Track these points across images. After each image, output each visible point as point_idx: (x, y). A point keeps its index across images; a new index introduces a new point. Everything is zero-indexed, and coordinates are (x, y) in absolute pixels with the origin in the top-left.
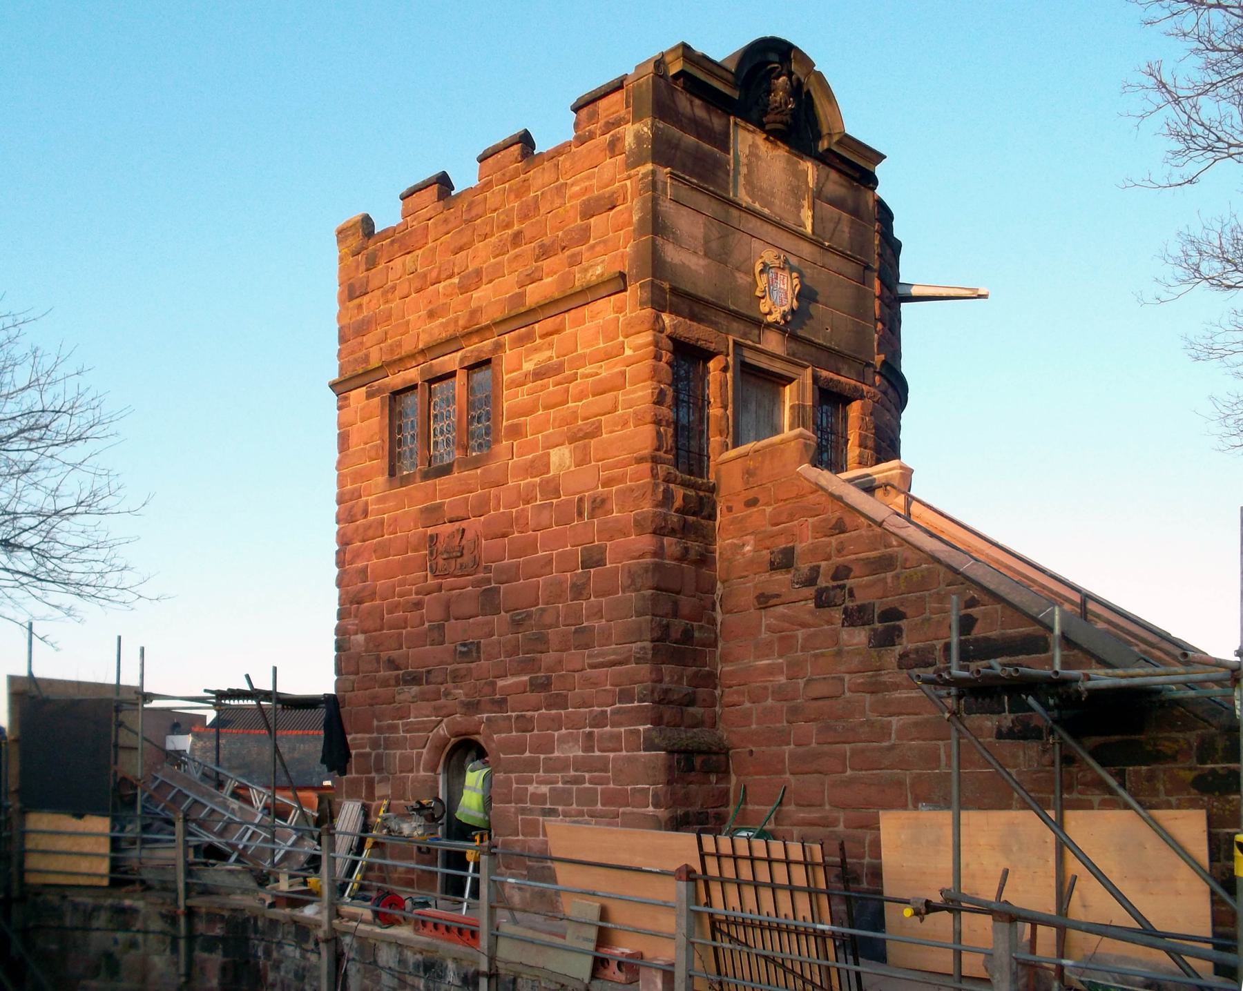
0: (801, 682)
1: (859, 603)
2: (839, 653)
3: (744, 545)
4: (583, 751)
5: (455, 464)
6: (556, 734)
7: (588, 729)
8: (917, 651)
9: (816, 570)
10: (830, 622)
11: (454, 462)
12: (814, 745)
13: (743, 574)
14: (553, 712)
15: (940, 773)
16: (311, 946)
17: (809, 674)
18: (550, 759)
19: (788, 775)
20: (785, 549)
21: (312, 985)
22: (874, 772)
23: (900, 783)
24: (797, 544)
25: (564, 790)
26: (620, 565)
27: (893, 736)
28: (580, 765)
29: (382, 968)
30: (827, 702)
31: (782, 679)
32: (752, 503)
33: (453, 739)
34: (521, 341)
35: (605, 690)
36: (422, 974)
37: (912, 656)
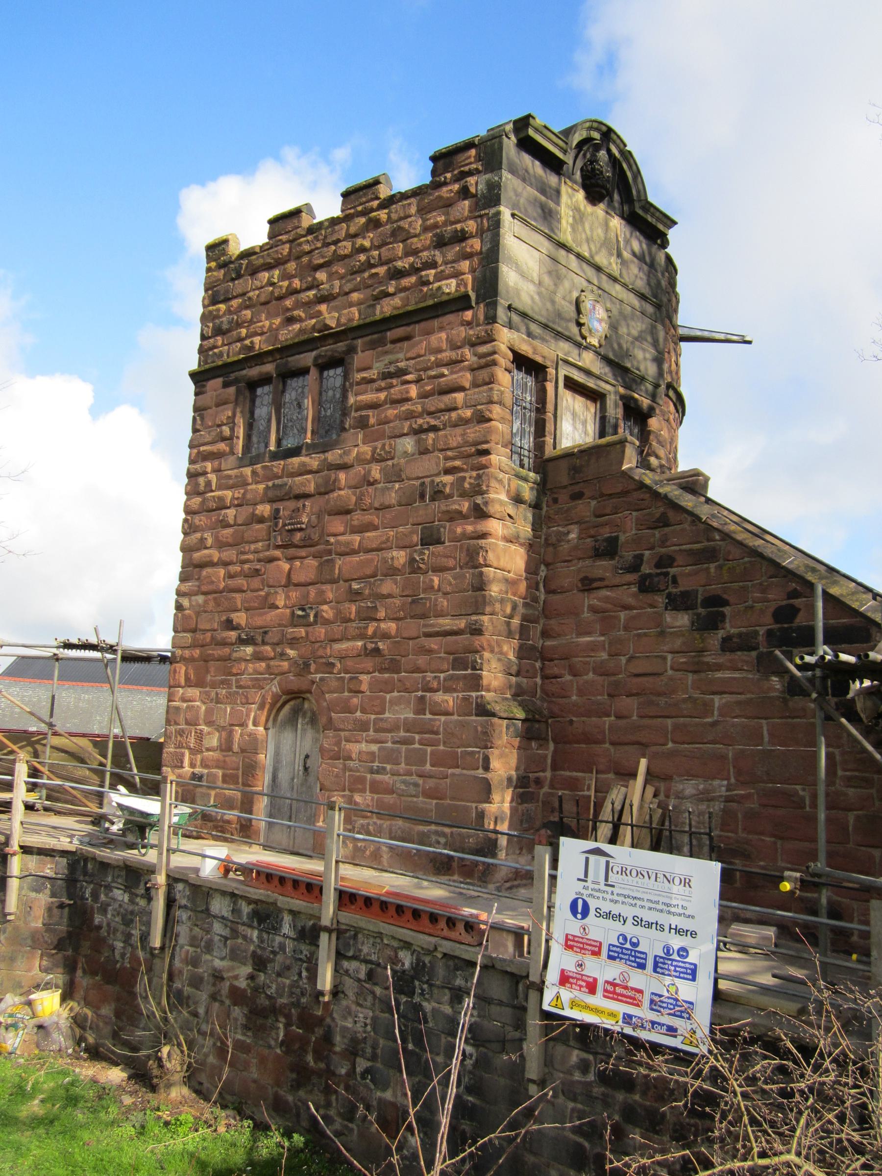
0: (623, 659)
1: (681, 589)
2: (662, 634)
3: (569, 532)
4: (415, 714)
5: (304, 448)
6: (388, 696)
7: (420, 693)
8: (740, 635)
9: (639, 558)
10: (652, 606)
11: (302, 445)
12: (635, 718)
13: (567, 558)
14: (386, 675)
15: (763, 750)
16: (141, 891)
17: (631, 652)
18: (382, 719)
19: (607, 745)
20: (610, 537)
22: (697, 746)
23: (723, 757)
25: (392, 750)
26: (459, 544)
27: (716, 713)
28: (409, 726)
29: (215, 917)
30: (650, 679)
31: (604, 655)
32: (577, 496)
33: (284, 697)
34: (372, 346)
35: (440, 657)
36: (255, 924)
37: (735, 640)
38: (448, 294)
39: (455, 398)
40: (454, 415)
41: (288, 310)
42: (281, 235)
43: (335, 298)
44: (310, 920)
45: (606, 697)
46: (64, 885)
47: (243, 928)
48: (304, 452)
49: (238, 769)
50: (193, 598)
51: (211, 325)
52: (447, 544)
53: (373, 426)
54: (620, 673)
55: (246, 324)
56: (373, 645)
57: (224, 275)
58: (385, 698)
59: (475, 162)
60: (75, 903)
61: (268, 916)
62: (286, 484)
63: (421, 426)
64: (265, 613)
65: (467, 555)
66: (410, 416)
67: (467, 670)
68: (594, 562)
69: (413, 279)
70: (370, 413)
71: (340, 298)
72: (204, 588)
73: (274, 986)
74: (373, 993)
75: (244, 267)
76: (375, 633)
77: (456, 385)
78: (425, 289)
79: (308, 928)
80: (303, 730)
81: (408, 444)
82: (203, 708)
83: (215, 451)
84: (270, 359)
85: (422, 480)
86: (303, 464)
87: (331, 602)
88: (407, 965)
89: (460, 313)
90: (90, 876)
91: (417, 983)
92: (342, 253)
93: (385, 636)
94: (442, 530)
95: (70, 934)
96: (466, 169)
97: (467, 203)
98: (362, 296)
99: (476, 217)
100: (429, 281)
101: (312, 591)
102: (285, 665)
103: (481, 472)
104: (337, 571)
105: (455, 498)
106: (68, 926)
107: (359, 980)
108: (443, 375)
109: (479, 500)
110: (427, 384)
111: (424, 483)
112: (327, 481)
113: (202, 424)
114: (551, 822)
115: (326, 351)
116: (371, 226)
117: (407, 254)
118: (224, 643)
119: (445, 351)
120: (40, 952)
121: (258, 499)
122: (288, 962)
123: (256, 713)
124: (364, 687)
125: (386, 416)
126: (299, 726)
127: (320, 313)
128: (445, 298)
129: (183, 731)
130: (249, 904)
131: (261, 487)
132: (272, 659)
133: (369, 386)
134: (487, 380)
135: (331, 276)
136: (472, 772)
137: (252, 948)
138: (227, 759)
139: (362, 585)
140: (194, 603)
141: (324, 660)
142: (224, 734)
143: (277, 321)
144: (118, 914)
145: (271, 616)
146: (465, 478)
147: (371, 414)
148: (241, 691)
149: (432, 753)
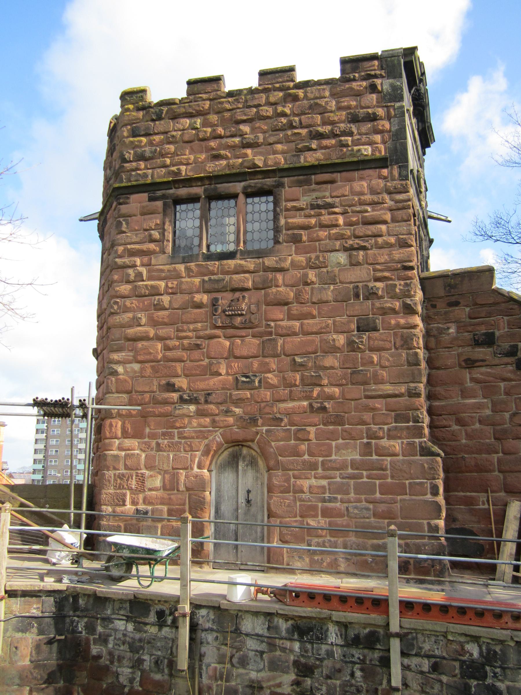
0: (507, 415)
3: (448, 328)
4: (360, 455)
6: (334, 443)
7: (365, 440)
13: (449, 346)
19: (497, 473)
21: (151, 655)
24: (496, 331)
25: (342, 483)
28: (354, 465)
29: (247, 635)
31: (488, 412)
33: (225, 445)
34: (300, 184)
35: (383, 414)
36: (296, 636)
38: (366, 155)
39: (381, 228)
40: (380, 240)
41: (213, 149)
42: (201, 94)
43: (259, 146)
44: (365, 628)
45: (493, 440)
46: (52, 622)
47: (281, 642)
48: (238, 256)
49: (184, 504)
50: (128, 366)
51: (132, 152)
52: (381, 331)
53: (305, 242)
54: (506, 424)
55: (169, 156)
56: (319, 405)
57: (143, 116)
58: (331, 445)
59: (378, 70)
60: (66, 637)
61: (311, 629)
62: (224, 280)
63: (352, 245)
64: (208, 379)
65: (402, 340)
66: (341, 237)
67: (408, 423)
68: (473, 348)
69: (333, 141)
70: (302, 232)
71: (263, 146)
72: (140, 358)
73: (324, 688)
74: (440, 681)
75: (164, 112)
76: (318, 395)
77: (381, 219)
78: (345, 150)
79: (362, 635)
80: (245, 471)
81: (342, 258)
82: (144, 455)
83: (145, 249)
84: (199, 184)
85: (356, 284)
86: (241, 266)
87: (274, 371)
88: (476, 654)
89: (377, 170)
90: (82, 611)
91: (488, 668)
92: (265, 114)
93: (330, 397)
94: (377, 321)
95: (60, 667)
96: (373, 73)
97: (374, 96)
98: (286, 148)
99: (383, 107)
100: (348, 144)
101: (256, 364)
102: (231, 420)
103: (408, 281)
104: (279, 348)
105: (386, 299)
106: (57, 660)
107: (422, 673)
108: (367, 211)
109: (408, 301)
110: (353, 217)
111: (358, 286)
112: (265, 281)
113: (127, 228)
114: (453, 528)
115: (256, 183)
116: (290, 99)
117: (324, 123)
118: (166, 402)
119: (366, 194)
120: (28, 688)
121: (195, 290)
122: (338, 666)
123: (200, 458)
124: (312, 436)
125: (318, 236)
126: (240, 468)
127: (246, 155)
128: (362, 158)
129: (123, 475)
130: (287, 620)
131: (197, 281)
132: (217, 415)
133: (298, 213)
134: (405, 218)
135: (253, 130)
136: (421, 497)
137: (292, 658)
138: (172, 496)
139: (305, 359)
140: (129, 370)
141: (271, 416)
142: (167, 476)
143: (203, 156)
144: (124, 644)
145: (213, 382)
146: (396, 285)
147: (303, 233)
148: (183, 441)
149: (380, 485)
